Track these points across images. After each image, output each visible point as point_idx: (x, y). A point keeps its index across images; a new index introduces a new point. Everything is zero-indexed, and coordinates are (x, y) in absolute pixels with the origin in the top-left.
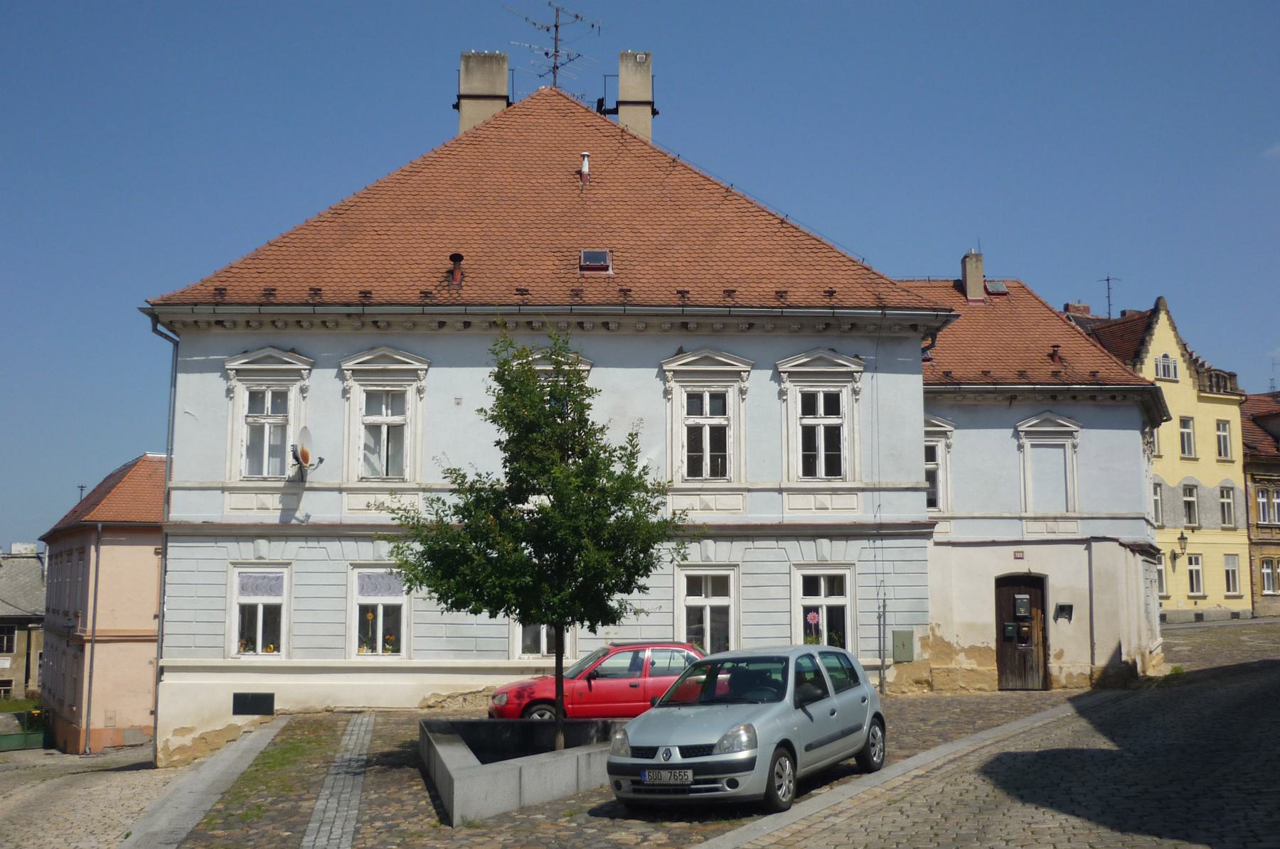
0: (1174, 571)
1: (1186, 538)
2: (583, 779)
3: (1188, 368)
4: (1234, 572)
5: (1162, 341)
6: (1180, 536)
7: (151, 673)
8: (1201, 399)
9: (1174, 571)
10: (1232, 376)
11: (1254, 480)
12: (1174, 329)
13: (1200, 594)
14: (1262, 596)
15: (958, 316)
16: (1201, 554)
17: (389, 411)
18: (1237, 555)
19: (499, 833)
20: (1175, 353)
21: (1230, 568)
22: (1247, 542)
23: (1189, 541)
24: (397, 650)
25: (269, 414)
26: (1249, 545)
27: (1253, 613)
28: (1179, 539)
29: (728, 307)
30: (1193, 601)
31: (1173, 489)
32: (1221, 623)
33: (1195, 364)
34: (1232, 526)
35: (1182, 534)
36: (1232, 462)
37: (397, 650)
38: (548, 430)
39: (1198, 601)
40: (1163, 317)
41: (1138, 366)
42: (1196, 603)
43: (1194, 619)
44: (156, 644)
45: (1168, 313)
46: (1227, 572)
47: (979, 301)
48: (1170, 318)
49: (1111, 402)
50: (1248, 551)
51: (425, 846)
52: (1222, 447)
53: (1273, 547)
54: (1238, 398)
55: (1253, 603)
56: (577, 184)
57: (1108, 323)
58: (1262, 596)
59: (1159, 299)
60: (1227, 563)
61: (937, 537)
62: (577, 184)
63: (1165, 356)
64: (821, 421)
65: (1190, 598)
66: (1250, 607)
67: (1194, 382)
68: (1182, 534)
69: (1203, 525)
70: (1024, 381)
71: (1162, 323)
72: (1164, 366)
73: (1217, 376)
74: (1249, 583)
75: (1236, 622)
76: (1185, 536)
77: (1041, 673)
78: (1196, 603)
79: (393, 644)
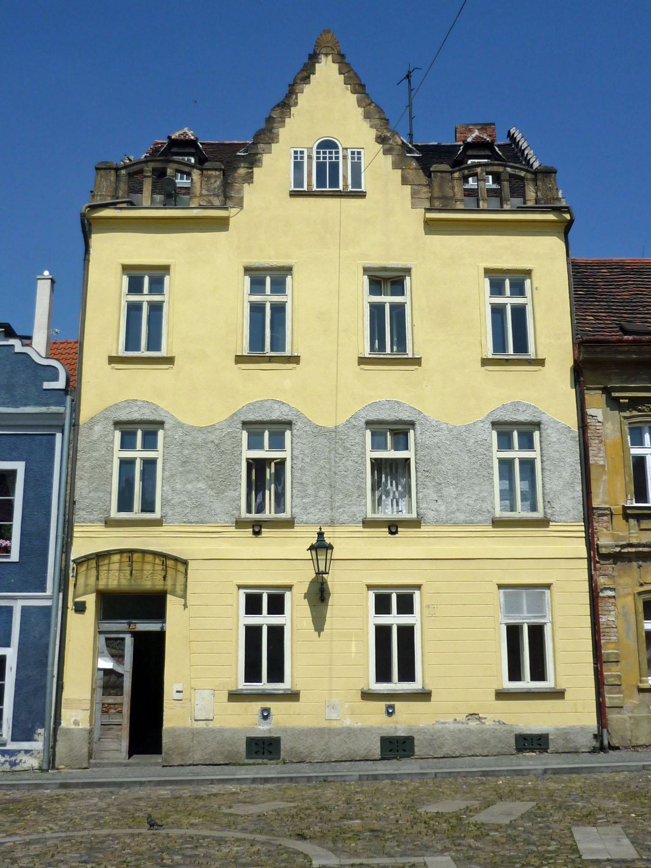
0: (319, 624)
1: (330, 547)
4: (537, 632)
8: (431, 227)
9: (319, 624)
11: (614, 403)
13: (414, 687)
16: (418, 587)
17: (395, 348)
18: (548, 586)
21: (525, 620)
22: (581, 549)
23: (336, 554)
25: (315, 188)
26: (590, 559)
27: (598, 737)
28: (311, 548)
30: (382, 705)
31: (332, 435)
32: (481, 764)
34: (539, 515)
35: (321, 534)
36: (540, 362)
39: (398, 705)
43: (377, 751)
46: (513, 632)
50: (586, 576)
54: (551, 217)
55: (601, 709)
58: (641, 690)
60: (511, 606)
64: (508, 301)
65: (367, 696)
66: (591, 721)
67: (414, 194)
68: (321, 534)
69: (430, 515)
74: (590, 658)
75: (532, 761)
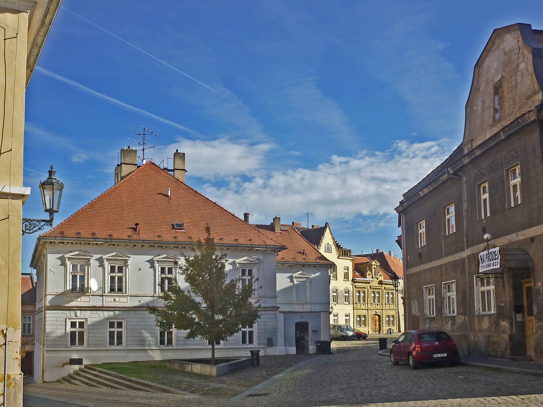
3: (336, 248)
5: (327, 238)
10: (350, 251)
12: (331, 234)
15: (287, 248)
19: (196, 387)
20: (331, 242)
23: (334, 308)
29: (222, 244)
33: (338, 246)
40: (328, 229)
41: (319, 247)
44: (345, 324)
45: (329, 228)
47: (279, 233)
48: (330, 230)
49: (320, 268)
51: (139, 403)
52: (346, 276)
56: (166, 199)
57: (308, 230)
59: (326, 223)
61: (280, 310)
62: (166, 199)
63: (328, 244)
70: (295, 261)
71: (327, 234)
72: (328, 247)
73: (345, 251)
79: (120, 343)
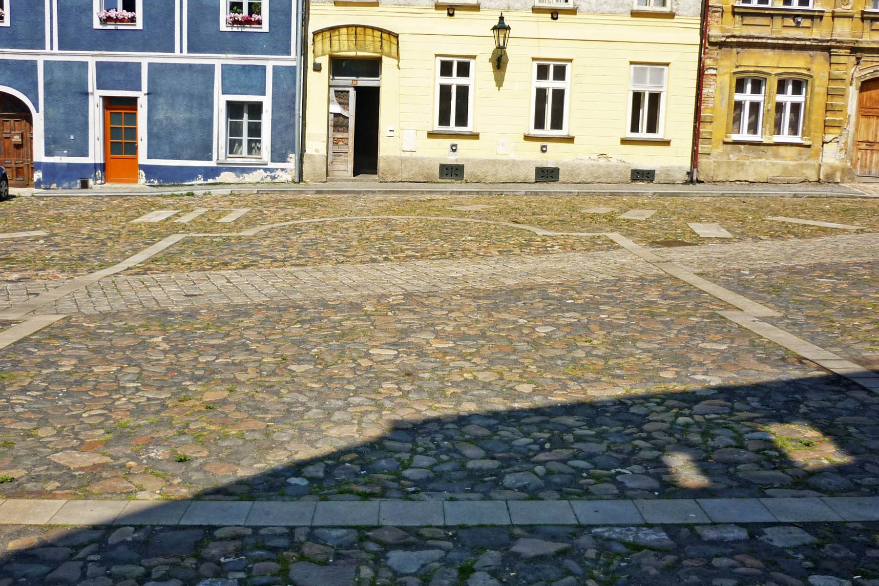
1: (509, 28)
2: (327, 41)
4: (655, 98)
6: (496, 23)
7: (823, 126)
14: (725, 143)
18: (667, 64)
23: (512, 33)
24: (755, 132)
28: (495, 28)
30: (538, 145)
37: (755, 132)
38: (50, 136)
39: (550, 145)
42: (543, 150)
43: (533, 177)
46: (637, 97)
53: (770, 53)
58: (725, 143)
66: (687, 164)
75: (641, 187)
76: (507, 23)
77: (160, 198)
78: (543, 150)
